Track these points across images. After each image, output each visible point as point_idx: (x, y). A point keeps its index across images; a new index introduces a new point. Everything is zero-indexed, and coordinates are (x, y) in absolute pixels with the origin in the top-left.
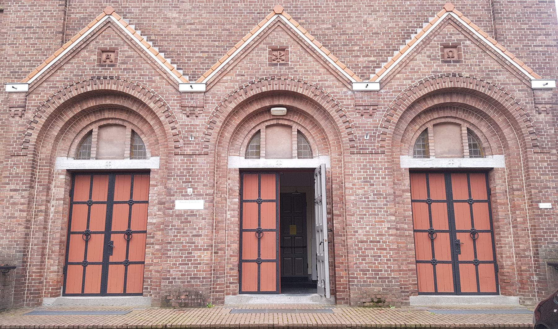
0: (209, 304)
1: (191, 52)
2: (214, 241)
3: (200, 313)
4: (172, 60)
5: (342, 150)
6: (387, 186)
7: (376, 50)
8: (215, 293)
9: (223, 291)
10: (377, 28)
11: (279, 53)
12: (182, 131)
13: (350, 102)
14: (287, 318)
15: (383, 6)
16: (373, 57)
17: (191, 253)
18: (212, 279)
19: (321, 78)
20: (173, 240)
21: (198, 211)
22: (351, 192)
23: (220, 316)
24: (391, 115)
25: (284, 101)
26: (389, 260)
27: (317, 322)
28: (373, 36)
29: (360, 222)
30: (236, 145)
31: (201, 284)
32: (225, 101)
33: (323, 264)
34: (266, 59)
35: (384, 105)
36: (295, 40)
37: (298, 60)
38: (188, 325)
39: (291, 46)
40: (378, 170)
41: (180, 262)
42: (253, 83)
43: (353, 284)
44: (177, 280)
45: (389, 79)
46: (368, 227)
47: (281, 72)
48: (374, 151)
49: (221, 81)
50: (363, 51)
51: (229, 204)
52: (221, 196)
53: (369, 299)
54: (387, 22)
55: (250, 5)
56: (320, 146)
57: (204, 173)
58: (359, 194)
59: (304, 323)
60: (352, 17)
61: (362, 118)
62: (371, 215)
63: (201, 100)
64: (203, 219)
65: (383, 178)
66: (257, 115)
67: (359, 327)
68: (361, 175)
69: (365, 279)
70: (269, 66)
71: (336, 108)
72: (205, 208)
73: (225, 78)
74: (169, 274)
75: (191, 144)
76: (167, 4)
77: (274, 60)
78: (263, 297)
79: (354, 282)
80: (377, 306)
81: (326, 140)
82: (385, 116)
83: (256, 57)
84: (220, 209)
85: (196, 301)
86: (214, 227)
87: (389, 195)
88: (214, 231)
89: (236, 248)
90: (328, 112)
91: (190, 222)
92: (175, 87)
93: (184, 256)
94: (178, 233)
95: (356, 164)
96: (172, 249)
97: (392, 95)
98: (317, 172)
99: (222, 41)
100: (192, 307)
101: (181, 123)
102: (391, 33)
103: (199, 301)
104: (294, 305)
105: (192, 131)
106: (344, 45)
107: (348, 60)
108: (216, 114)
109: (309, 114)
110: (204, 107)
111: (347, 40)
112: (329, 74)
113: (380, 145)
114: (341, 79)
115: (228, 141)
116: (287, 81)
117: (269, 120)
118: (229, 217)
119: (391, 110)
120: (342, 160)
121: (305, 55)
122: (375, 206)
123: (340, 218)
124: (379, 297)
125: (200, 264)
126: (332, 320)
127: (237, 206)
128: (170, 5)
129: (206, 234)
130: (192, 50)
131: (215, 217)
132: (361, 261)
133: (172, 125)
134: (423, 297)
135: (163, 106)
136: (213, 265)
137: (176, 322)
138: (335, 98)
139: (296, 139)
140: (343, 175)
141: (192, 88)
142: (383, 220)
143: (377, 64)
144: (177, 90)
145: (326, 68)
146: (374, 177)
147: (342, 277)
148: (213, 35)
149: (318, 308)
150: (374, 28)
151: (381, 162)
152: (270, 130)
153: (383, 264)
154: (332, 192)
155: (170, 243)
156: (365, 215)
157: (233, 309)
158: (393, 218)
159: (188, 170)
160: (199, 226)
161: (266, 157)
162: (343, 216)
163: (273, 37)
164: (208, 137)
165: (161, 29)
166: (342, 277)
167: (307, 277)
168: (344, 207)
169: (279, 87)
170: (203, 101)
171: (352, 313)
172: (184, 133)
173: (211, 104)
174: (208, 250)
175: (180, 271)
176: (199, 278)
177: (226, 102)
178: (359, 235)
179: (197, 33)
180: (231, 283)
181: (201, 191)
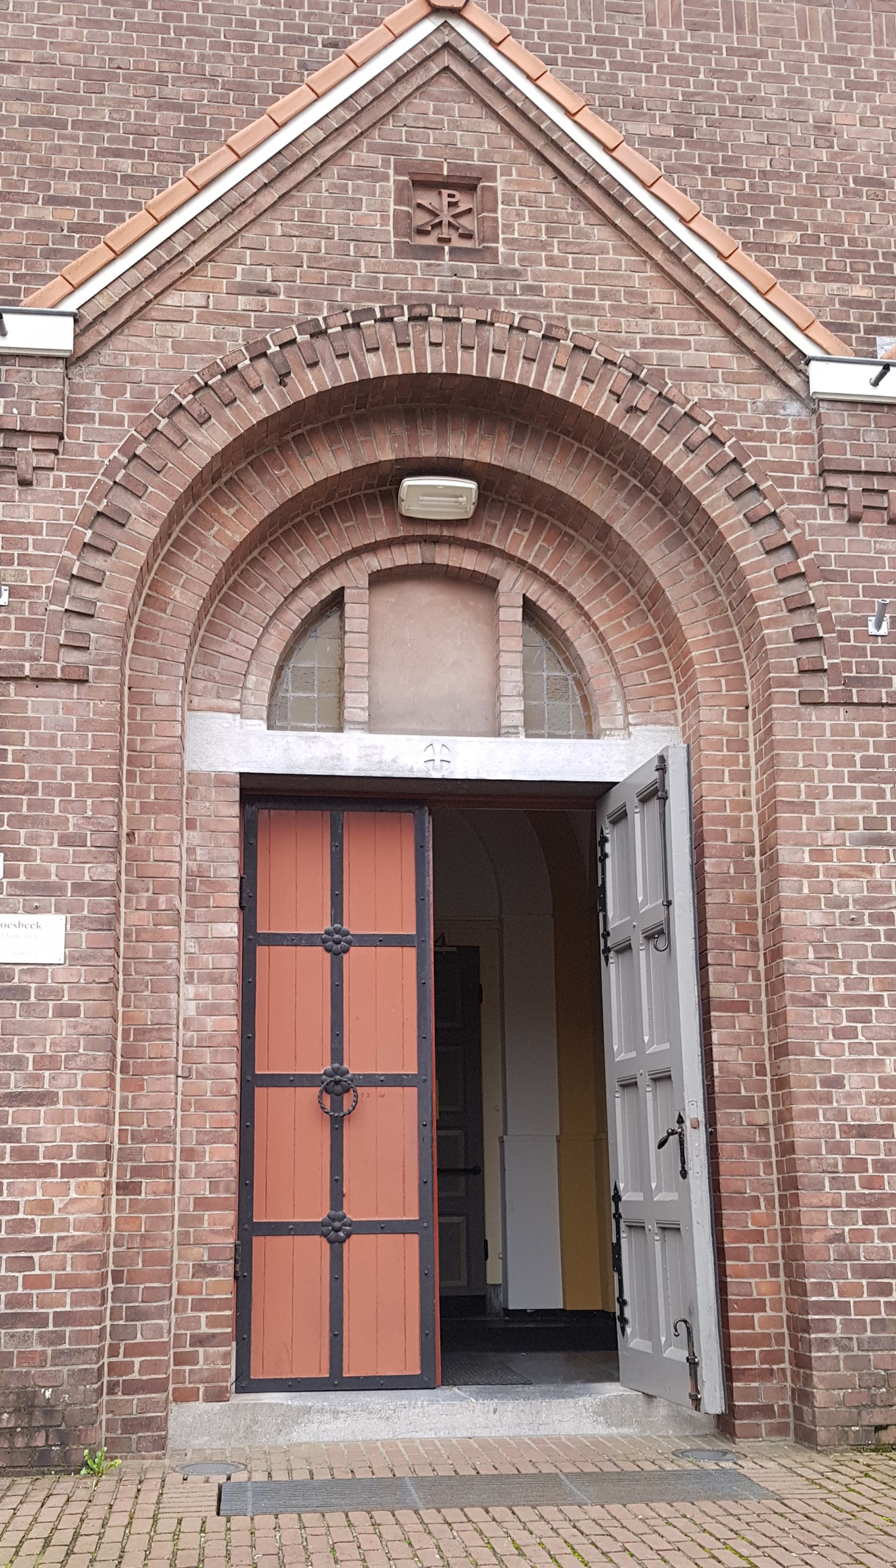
2: (117, 1127)
3: (49, 1514)
7: (875, 255)
8: (120, 1397)
9: (159, 1386)
10: (877, 159)
11: (446, 200)
13: (793, 453)
16: (865, 282)
18: (108, 1323)
19: (657, 330)
21: (31, 972)
22: (806, 890)
25: (467, 443)
29: (851, 1033)
30: (224, 661)
31: (49, 1350)
34: (384, 219)
36: (529, 146)
37: (544, 237)
39: (506, 172)
42: (318, 333)
43: (826, 1341)
47: (457, 287)
49: (154, 314)
50: (821, 251)
51: (191, 946)
52: (152, 905)
56: (630, 679)
57: (66, 775)
58: (846, 899)
60: (767, 102)
61: (854, 531)
64: (61, 1012)
66: (327, 513)
68: (853, 809)
69: (883, 1315)
70: (399, 253)
71: (731, 477)
72: (72, 959)
73: (173, 299)
77: (421, 232)
78: (364, 1408)
79: (828, 1326)
83: (336, 205)
85: (20, 1442)
86: (119, 1059)
88: (118, 1076)
89: (226, 1167)
95: (830, 754)
99: (154, 156)
103: (40, 1441)
108: (127, 475)
110: (61, 437)
111: (742, 197)
112: (694, 314)
114: (750, 341)
115: (189, 627)
116: (492, 336)
117: (388, 544)
118: (192, 1012)
121: (572, 215)
123: (743, 1020)
125: (43, 1244)
129: (79, 1088)
131: (121, 1009)
132: (860, 1225)
134: (434, 1297)
136: (112, 1249)
139: (516, 643)
145: (678, 285)
147: (760, 1305)
148: (108, 127)
150: (864, 159)
157: (222, 1479)
160: (39, 1049)
161: (373, 725)
162: (758, 1010)
164: (87, 591)
166: (760, 1305)
169: (452, 360)
173: (101, 422)
174: (86, 1171)
176: (40, 1320)
178: (849, 1097)
179: (30, 110)
180: (200, 1341)
181: (53, 867)
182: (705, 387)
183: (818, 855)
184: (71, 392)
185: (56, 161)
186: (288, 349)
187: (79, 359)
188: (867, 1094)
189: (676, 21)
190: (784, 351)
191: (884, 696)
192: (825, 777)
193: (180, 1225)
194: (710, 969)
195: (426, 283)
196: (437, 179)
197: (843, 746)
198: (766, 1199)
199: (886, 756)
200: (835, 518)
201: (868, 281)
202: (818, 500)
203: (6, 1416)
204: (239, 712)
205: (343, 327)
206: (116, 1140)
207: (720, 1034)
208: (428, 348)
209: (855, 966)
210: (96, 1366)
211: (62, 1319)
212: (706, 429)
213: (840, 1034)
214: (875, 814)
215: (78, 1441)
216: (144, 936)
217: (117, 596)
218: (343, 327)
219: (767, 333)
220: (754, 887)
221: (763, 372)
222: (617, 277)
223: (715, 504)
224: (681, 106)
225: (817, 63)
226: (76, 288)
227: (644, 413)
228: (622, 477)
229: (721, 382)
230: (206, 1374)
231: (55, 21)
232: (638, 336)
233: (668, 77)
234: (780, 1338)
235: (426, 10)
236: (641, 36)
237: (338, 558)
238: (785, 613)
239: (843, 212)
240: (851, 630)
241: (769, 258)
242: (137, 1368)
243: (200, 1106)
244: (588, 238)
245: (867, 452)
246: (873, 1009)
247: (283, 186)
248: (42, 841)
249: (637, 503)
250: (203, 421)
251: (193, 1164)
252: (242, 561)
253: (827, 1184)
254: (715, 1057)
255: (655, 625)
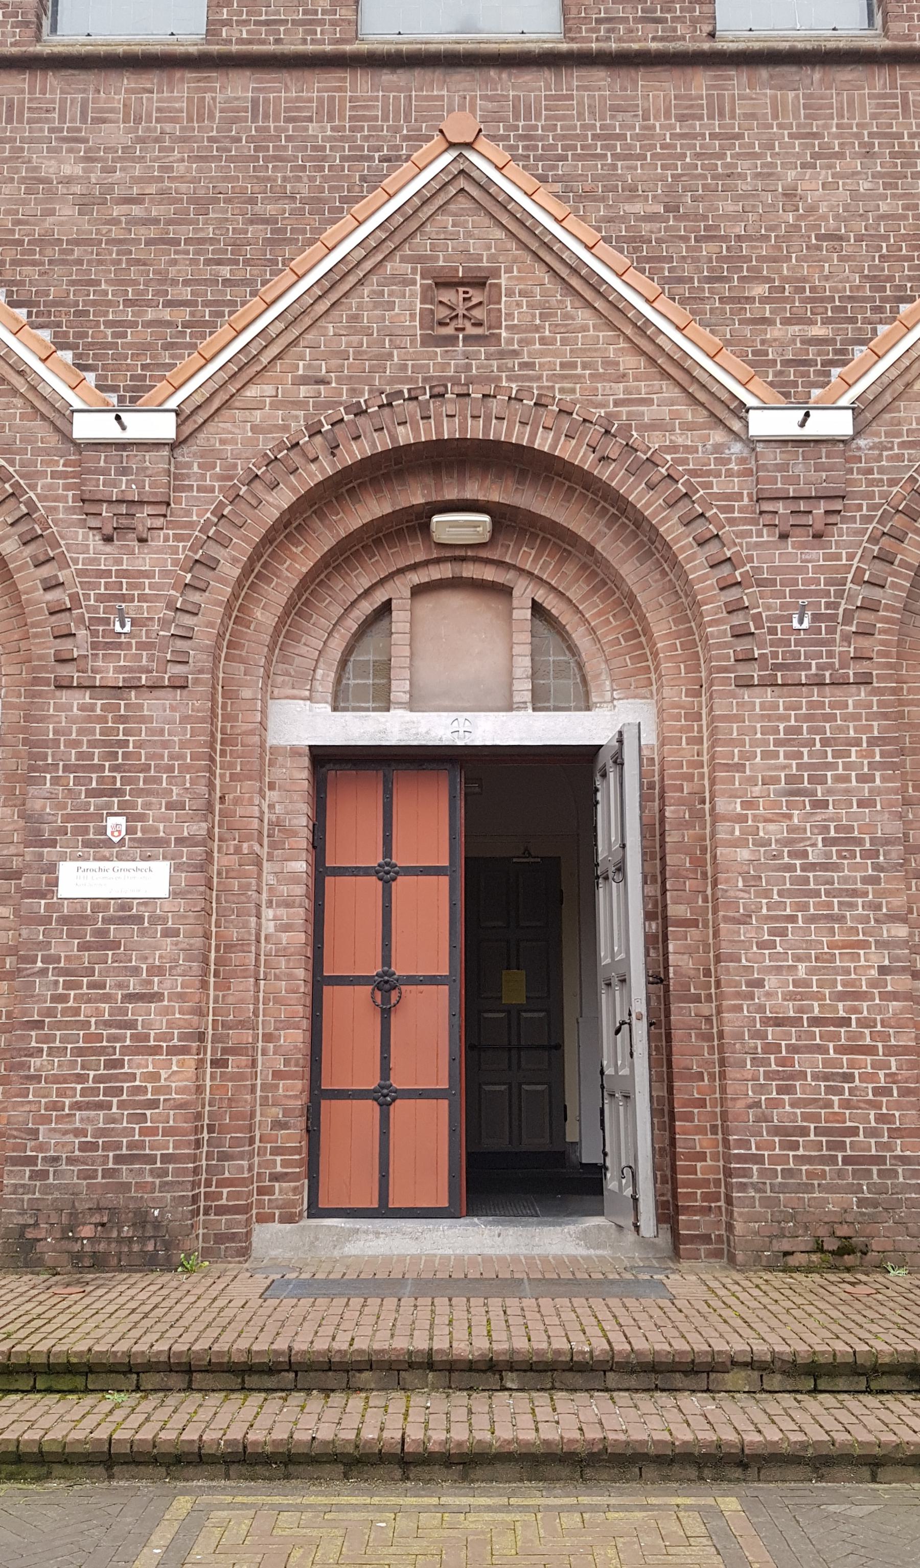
0: (188, 1258)
1: (128, 303)
2: (211, 1018)
4: (56, 335)
5: (703, 674)
6: (879, 807)
8: (212, 1217)
9: (246, 1209)
10: (837, 217)
11: (462, 296)
12: (87, 597)
14: (488, 1320)
15: (858, 136)
16: (823, 323)
17: (119, 1064)
18: (204, 1163)
19: (626, 391)
20: (51, 1012)
22: (737, 833)
23: (222, 1309)
24: (899, 534)
25: (480, 489)
26: (887, 1092)
27: (609, 1343)
28: (819, 248)
29: (772, 945)
30: (298, 660)
32: (251, 481)
33: (626, 1107)
34: (413, 317)
35: (870, 495)
36: (527, 247)
37: (538, 322)
38: (80, 1354)
39: (509, 270)
40: (842, 749)
41: (78, 1098)
43: (745, 1184)
44: (64, 1167)
45: (888, 398)
46: (802, 967)
47: (468, 367)
48: (827, 674)
50: (785, 300)
51: (272, 880)
52: (238, 851)
53: (805, 1241)
54: (871, 196)
55: (352, 129)
56: (616, 662)
57: (171, 758)
58: (770, 839)
59: (556, 1345)
62: (813, 919)
63: (158, 474)
64: (166, 934)
65: (862, 779)
66: (378, 542)
67: (783, 1361)
69: (792, 1166)
70: (423, 344)
71: (683, 508)
72: (174, 894)
73: (252, 392)
74: (33, 1143)
75: (119, 646)
76: (41, 130)
77: (441, 324)
80: (836, 1268)
81: (643, 639)
82: (873, 540)
84: (235, 898)
85: (136, 1248)
86: (213, 967)
87: (887, 842)
88: (212, 980)
90: (652, 526)
91: (115, 945)
92: (58, 423)
93: (92, 1073)
94: (68, 986)
95: (758, 725)
96: (45, 1046)
97: (900, 458)
98: (604, 758)
100: (121, 1269)
101: (80, 566)
102: (886, 238)
104: (516, 1259)
105: (123, 598)
106: (709, 280)
107: (728, 336)
108: (217, 531)
109: (574, 535)
110: (168, 504)
111: (721, 259)
112: (658, 377)
113: (852, 649)
114: (701, 396)
115: (267, 639)
116: (495, 406)
117: (426, 563)
118: (271, 930)
119: (897, 517)
120: (704, 711)
121: (561, 301)
122: (833, 883)
123: (694, 933)
124: (843, 1231)
125: (154, 1104)
126: (671, 1333)
127: (300, 890)
128: (51, 130)
129: (179, 989)
130: (130, 297)
131: (214, 929)
132: (774, 1095)
133: (46, 571)
135: (12, 499)
136: (207, 1108)
137: (34, 1339)
138: (680, 468)
139: (526, 637)
140: (706, 770)
141: (124, 428)
142: (861, 937)
143: (836, 352)
144: (67, 438)
145: (644, 353)
146: (829, 774)
147: (702, 1157)
148: (212, 241)
149: (611, 1277)
150: (825, 218)
151: (856, 717)
152: (427, 605)
153: (862, 1105)
154: (662, 834)
155: (39, 1025)
156: (792, 919)
158: (901, 931)
159: (111, 746)
160: (150, 961)
161: (412, 705)
162: (706, 926)
163: (437, 233)
164: (188, 620)
165: (17, 222)
166: (702, 1157)
167: (563, 1153)
168: (709, 892)
169: (463, 427)
170: (165, 479)
171: (743, 1296)
172: (92, 602)
174: (184, 1051)
175: (78, 1132)
176: (151, 1159)
177: (257, 485)
178: (768, 995)
180: (275, 1177)
181: (161, 826)
182: (664, 436)
183: (746, 805)
184: (176, 468)
185: (172, 271)
186: (337, 427)
187: (181, 443)
188: (782, 993)
189: (667, 116)
190: (728, 403)
191: (803, 678)
192: (754, 743)
193: (261, 1091)
194: (668, 893)
195: (444, 367)
196: (456, 280)
197: (769, 718)
198: (709, 1074)
199: (805, 725)
200: (768, 536)
201: (826, 322)
202: (754, 522)
203: (126, 1228)
204: (310, 699)
205: (379, 407)
206: (210, 1027)
207: (675, 945)
208: (445, 419)
209: (775, 892)
210: (190, 1194)
211: (166, 1159)
212: (663, 471)
213: (761, 945)
214: (794, 772)
215: (177, 1247)
216: (231, 874)
217: (210, 622)
218: (379, 407)
219: (715, 388)
220: (705, 828)
221: (713, 419)
222: (596, 350)
223: (669, 531)
224: (670, 186)
225: (787, 139)
226: (177, 389)
227: (614, 460)
228: (603, 507)
229: (678, 431)
230: (280, 1202)
231: (171, 159)
232: (611, 398)
233: (659, 163)
234: (717, 1182)
235: (445, 145)
236: (637, 131)
237: (386, 577)
238: (725, 614)
239: (805, 265)
240: (779, 626)
241: (741, 308)
242: (225, 1196)
243: (276, 1001)
244: (574, 319)
245: (795, 480)
246: (790, 926)
247: (334, 296)
248: (153, 807)
249: (615, 528)
250: (274, 486)
251: (271, 1045)
252: (312, 583)
253: (749, 1063)
254: (671, 963)
255: (635, 619)
